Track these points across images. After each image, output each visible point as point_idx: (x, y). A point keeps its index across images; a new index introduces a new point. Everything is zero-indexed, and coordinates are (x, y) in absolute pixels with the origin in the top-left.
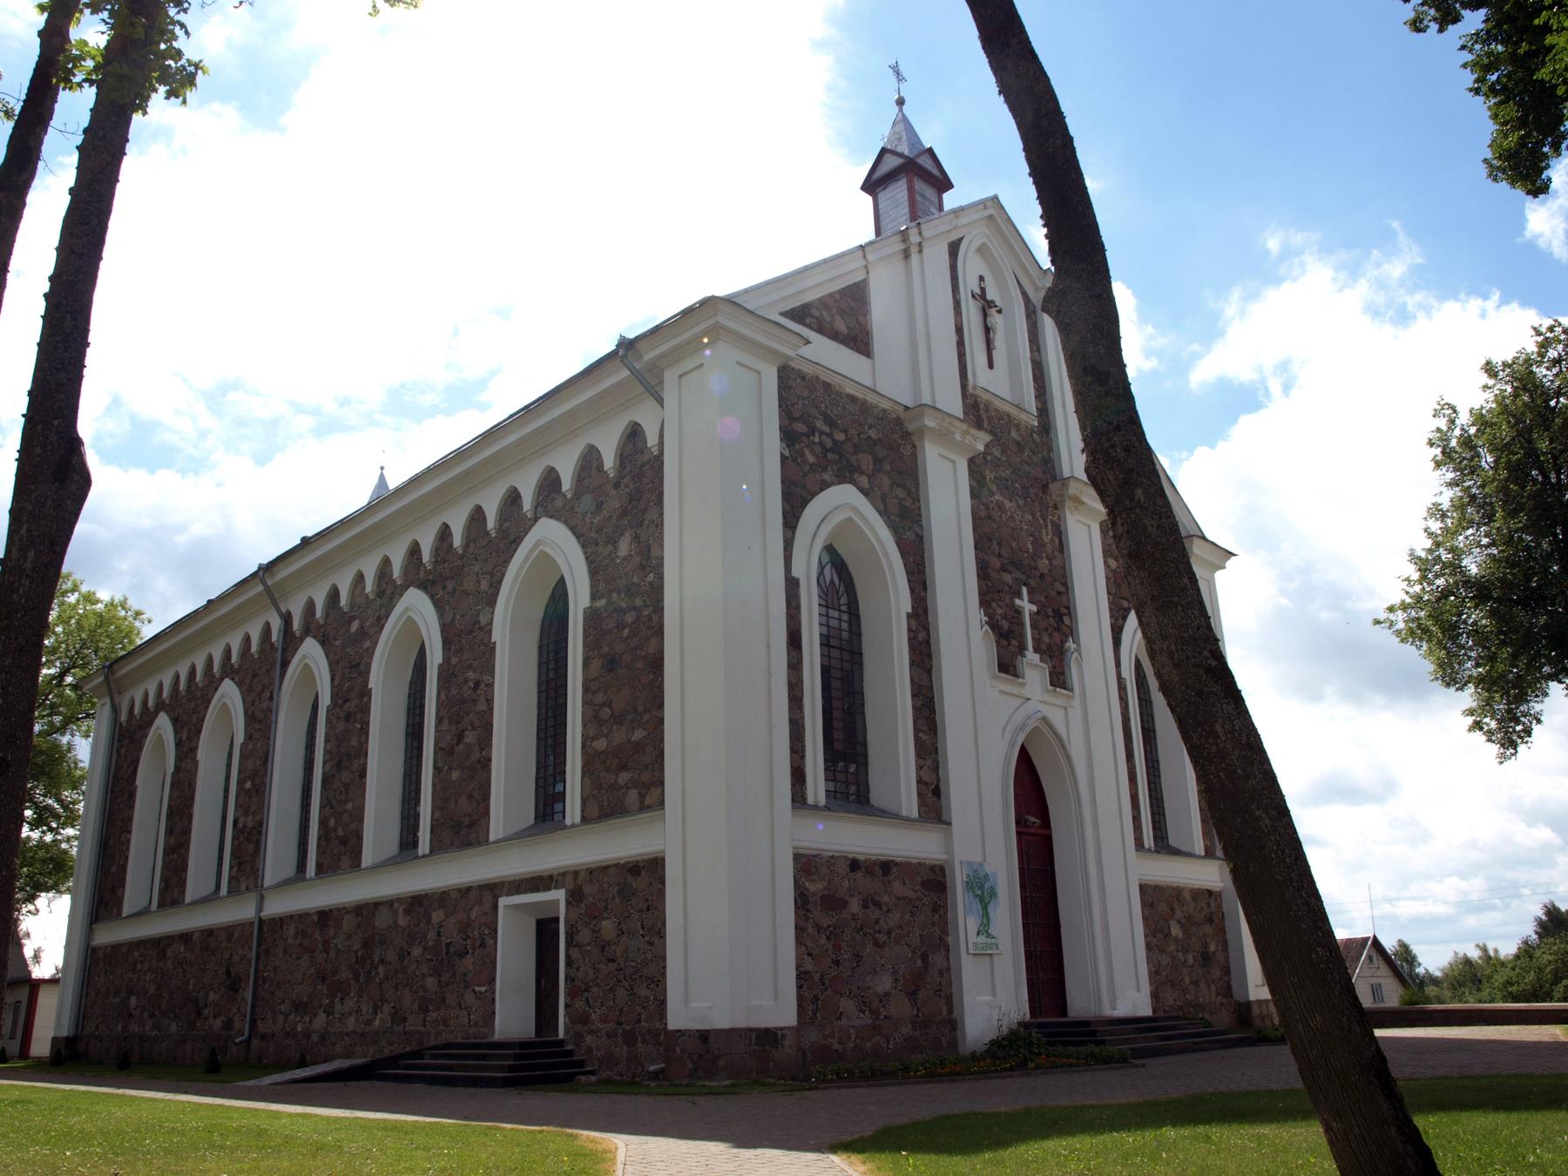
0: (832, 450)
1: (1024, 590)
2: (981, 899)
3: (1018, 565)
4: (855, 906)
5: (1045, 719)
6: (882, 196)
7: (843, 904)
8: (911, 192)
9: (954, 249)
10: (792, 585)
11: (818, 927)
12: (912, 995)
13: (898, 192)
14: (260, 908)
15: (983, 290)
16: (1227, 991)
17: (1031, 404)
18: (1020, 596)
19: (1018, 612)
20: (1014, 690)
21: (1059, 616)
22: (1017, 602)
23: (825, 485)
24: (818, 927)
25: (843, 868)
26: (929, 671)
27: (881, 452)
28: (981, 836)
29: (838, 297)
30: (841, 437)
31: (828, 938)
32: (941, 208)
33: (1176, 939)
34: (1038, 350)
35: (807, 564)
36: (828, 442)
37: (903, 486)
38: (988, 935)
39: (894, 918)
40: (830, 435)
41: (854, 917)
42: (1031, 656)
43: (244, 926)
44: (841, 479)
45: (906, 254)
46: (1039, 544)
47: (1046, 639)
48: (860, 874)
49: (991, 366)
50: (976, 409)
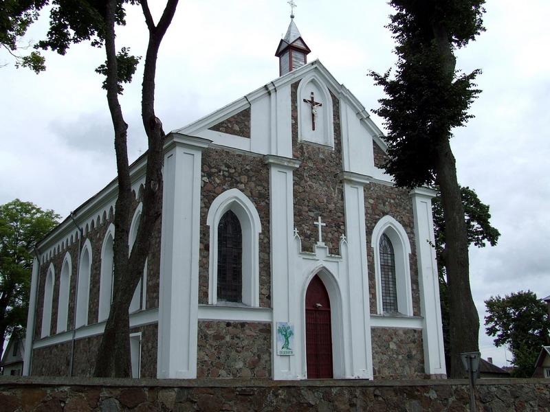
0: (228, 177)
1: (320, 218)
2: (285, 336)
3: (317, 208)
4: (228, 338)
5: (324, 267)
6: (283, 58)
7: (223, 338)
8: (291, 57)
9: (295, 86)
10: (205, 232)
11: (211, 346)
12: (253, 369)
13: (286, 57)
14: (74, 336)
15: (312, 98)
16: (423, 370)
17: (332, 142)
18: (317, 220)
19: (316, 227)
20: (311, 257)
21: (338, 226)
22: (315, 223)
23: (224, 190)
24: (211, 346)
25: (223, 325)
26: (269, 254)
27: (251, 173)
28: (289, 310)
29: (236, 117)
30: (232, 171)
31: (215, 350)
32: (305, 62)
33: (392, 350)
34: (339, 118)
35: (214, 221)
36: (226, 174)
37: (261, 185)
38: (288, 348)
39: (246, 342)
40: (228, 171)
41: (227, 342)
42: (321, 243)
43: (70, 342)
44: (231, 187)
45: (269, 93)
46: (330, 199)
47: (330, 235)
48: (231, 328)
49: (314, 129)
50: (300, 148)
